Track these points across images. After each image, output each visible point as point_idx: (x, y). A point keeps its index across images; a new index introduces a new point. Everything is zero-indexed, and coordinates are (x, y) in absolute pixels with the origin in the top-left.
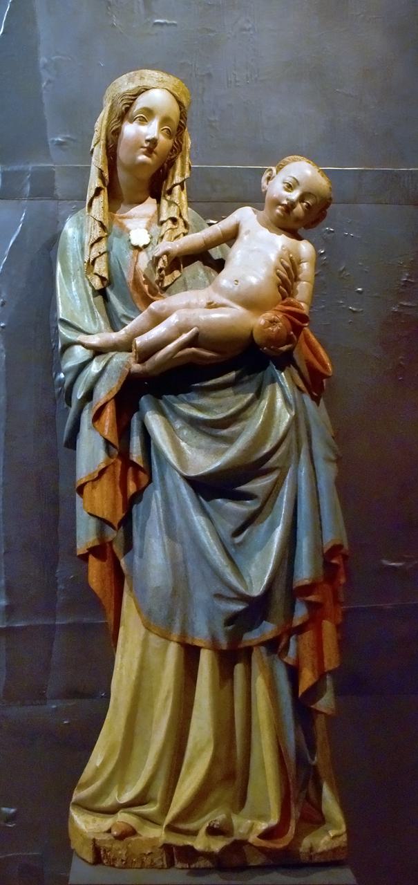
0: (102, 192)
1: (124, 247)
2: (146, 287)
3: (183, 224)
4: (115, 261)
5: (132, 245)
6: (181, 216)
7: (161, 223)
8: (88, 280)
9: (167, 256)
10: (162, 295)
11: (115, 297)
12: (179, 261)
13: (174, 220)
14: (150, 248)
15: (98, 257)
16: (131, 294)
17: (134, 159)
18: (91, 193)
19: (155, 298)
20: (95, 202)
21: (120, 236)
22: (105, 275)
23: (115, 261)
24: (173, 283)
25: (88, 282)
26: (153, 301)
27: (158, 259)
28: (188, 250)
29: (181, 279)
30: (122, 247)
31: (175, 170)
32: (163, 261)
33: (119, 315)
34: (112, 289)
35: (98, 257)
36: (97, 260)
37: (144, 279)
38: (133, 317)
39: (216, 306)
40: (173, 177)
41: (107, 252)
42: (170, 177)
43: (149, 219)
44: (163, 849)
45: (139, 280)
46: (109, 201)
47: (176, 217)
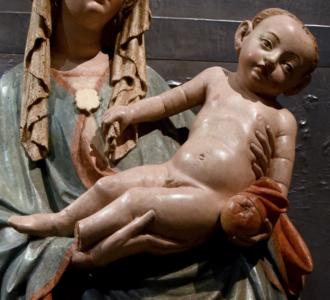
0: (44, 44)
1: (69, 110)
3: (140, 85)
4: (57, 128)
5: (78, 109)
6: (137, 75)
7: (113, 84)
8: (25, 149)
9: (120, 123)
10: (112, 169)
11: (55, 169)
13: (129, 81)
14: (99, 112)
15: (36, 122)
16: (75, 168)
17: (83, 6)
18: (30, 45)
19: (103, 173)
20: (35, 55)
21: (63, 97)
22: (45, 143)
23: (57, 128)
24: (125, 156)
25: (24, 152)
26: (101, 176)
27: (106, 127)
28: (145, 117)
29: (136, 151)
31: (131, 20)
33: (60, 192)
34: (52, 160)
35: (36, 122)
36: (36, 125)
37: (91, 150)
38: (76, 194)
39: (177, 185)
40: (129, 28)
41: (49, 116)
42: (126, 29)
43: (98, 78)
44: (52, 162)
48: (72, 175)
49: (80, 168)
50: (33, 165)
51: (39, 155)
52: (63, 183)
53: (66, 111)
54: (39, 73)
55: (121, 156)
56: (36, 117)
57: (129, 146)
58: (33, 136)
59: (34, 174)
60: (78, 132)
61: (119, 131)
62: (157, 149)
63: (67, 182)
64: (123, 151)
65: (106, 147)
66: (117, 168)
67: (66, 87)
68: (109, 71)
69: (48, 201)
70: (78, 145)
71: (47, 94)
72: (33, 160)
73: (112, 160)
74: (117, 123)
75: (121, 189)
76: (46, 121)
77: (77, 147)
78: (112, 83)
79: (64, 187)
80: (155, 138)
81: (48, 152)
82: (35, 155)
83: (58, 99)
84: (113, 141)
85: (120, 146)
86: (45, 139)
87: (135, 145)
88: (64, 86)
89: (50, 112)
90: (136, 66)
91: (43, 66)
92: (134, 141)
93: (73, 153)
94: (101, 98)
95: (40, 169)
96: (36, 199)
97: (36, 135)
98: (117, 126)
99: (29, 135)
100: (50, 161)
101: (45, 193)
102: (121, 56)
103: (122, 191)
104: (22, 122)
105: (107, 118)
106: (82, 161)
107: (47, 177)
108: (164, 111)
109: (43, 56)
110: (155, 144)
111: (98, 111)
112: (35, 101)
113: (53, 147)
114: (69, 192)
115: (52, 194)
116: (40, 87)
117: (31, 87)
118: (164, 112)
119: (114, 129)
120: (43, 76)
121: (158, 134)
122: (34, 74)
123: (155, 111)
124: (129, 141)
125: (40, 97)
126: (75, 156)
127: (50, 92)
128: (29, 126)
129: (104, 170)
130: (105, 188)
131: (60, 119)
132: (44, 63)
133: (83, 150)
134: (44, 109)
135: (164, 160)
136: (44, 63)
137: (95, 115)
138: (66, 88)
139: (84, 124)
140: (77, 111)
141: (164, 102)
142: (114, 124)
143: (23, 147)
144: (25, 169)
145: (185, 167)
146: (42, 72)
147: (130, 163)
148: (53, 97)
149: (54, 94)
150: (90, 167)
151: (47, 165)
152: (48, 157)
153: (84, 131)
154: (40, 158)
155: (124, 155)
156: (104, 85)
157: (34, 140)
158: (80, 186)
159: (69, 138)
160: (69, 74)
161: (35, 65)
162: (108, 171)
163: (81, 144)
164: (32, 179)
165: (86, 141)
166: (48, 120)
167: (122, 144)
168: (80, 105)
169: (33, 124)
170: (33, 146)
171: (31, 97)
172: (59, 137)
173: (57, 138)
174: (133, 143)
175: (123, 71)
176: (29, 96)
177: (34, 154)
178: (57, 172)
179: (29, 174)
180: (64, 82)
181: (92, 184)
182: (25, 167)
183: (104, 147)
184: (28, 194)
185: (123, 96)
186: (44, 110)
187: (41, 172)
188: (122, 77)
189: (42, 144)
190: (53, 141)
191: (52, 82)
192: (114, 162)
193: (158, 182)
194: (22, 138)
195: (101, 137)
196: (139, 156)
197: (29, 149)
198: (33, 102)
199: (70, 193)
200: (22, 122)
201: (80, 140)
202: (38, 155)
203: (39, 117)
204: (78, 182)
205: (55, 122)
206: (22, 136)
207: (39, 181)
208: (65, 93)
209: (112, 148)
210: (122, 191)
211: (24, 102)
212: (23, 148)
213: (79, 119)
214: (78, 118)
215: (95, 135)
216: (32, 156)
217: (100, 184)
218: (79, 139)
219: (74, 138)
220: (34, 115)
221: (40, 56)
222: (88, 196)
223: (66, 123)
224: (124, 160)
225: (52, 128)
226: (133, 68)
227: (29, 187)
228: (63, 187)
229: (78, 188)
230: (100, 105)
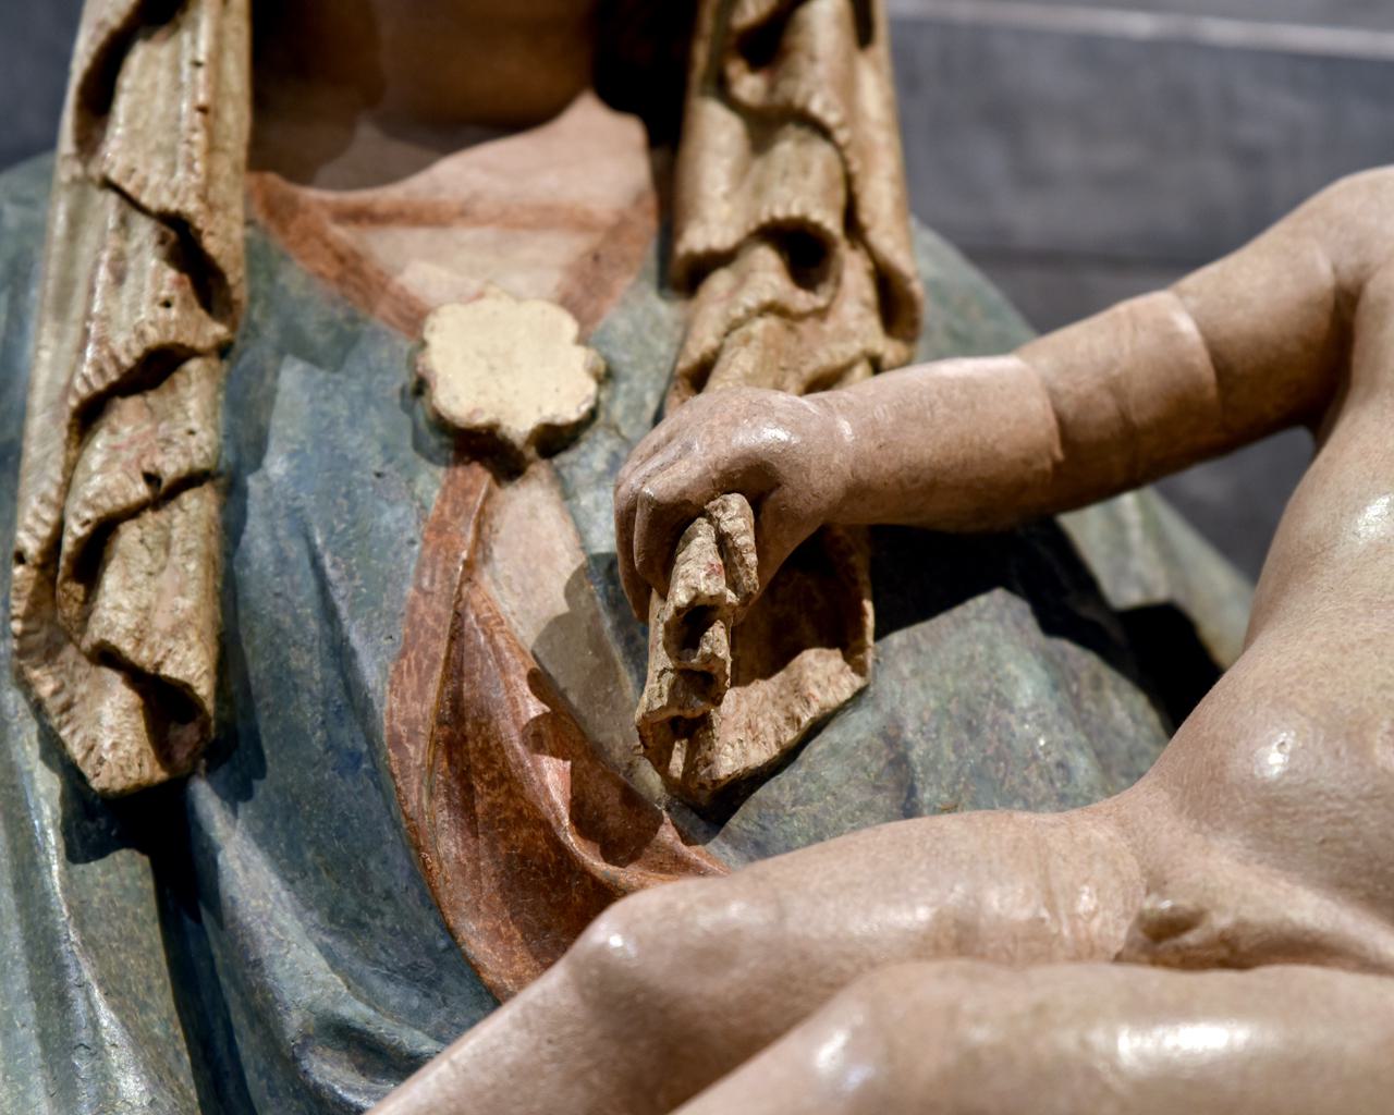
1: (372, 437)
2: (552, 777)
3: (869, 293)
4: (282, 560)
5: (442, 425)
6: (853, 225)
7: (686, 277)
8: (38, 707)
9: (757, 503)
10: (692, 853)
11: (258, 859)
12: (869, 562)
13: (804, 251)
14: (593, 455)
15: (133, 512)
16: (414, 843)
19: (626, 875)
20: (144, 67)
21: (337, 350)
22: (190, 665)
23: (282, 560)
24: (789, 756)
25: (32, 729)
26: (604, 895)
27: (662, 527)
28: (927, 484)
29: (858, 728)
30: (353, 441)
32: (723, 542)
33: (294, 1023)
34: (237, 793)
35: (133, 512)
36: (129, 534)
37: (534, 708)
38: (412, 1039)
39: (1239, 952)
41: (226, 480)
43: (580, 244)
44: (241, 806)
45: (485, 719)
46: (262, 100)
47: (816, 216)
48: (388, 895)
49: (448, 845)
50: (99, 821)
51: (141, 751)
52: (315, 954)
53: (353, 443)
54: (165, 178)
55: (759, 756)
56: (135, 482)
57: (815, 691)
58: (105, 614)
59: (100, 892)
60: (438, 586)
61: (752, 558)
62: (1012, 719)
63: (343, 949)
64: (774, 720)
65: (652, 684)
66: (728, 849)
67: (357, 288)
68: (651, 202)
69: (193, 1092)
70: (438, 674)
71: (218, 330)
72: (96, 784)
73: (693, 786)
74: (736, 502)
75: (792, 978)
76: (203, 513)
77: (432, 692)
78: (677, 272)
79: (324, 985)
80: (992, 646)
81: (209, 732)
82: (114, 746)
83: (300, 366)
84: (709, 634)
85: (746, 683)
86: (193, 638)
87: (859, 682)
88: (341, 280)
89: (238, 450)
90: (845, 162)
91: (194, 130)
92: (847, 659)
93: (402, 729)
94: (606, 358)
95: (146, 859)
96: (106, 1077)
97: (125, 603)
98: (740, 521)
99: (75, 608)
100: (224, 798)
101: (179, 1032)
102: (733, 105)
103: (798, 993)
104: (29, 521)
105: (662, 468)
106: (468, 789)
107: (198, 919)
108: (1059, 454)
109: (197, 64)
110: (992, 689)
111: (583, 447)
112: (131, 371)
113: (247, 690)
114: (359, 1023)
115: (231, 1042)
116: (171, 274)
117: (103, 274)
118: (1057, 465)
119: (713, 546)
120: (192, 196)
121: (1008, 622)
122: (129, 187)
123: (1002, 448)
124: (809, 656)
125: (171, 338)
126: (412, 749)
127: (242, 322)
128: (79, 541)
129: (633, 858)
130: (658, 970)
131: (307, 500)
132: (203, 110)
133: (472, 713)
134: (195, 425)
135: (1063, 798)
136: (203, 110)
137: (565, 472)
138: (357, 296)
139: (486, 530)
140: (433, 441)
141: (1053, 393)
142: (719, 514)
143: (27, 695)
144: (34, 856)
145: (1285, 816)
146: (190, 167)
147: (826, 811)
148: (256, 352)
149: (271, 331)
150: (525, 833)
151: (199, 828)
152: (208, 770)
153: (485, 577)
154: (150, 771)
155: (776, 751)
156: (623, 283)
157: (113, 639)
158: (449, 981)
159: (369, 624)
160: (380, 209)
161: (139, 124)
162: (660, 868)
163: (461, 673)
164: (81, 925)
165: (496, 648)
166: (223, 508)
167: (766, 675)
168: (456, 398)
169: (105, 531)
170: (101, 687)
171: (102, 342)
172: (295, 617)
173: (279, 630)
174: (842, 671)
175: (759, 191)
176: (86, 332)
177: (107, 743)
178: (275, 881)
179: (65, 890)
180: (341, 259)
181: (536, 958)
182: (32, 836)
183: (630, 691)
184: (43, 1037)
185: (767, 347)
186: (192, 433)
187: (149, 884)
188: (752, 227)
189: (169, 670)
190: (248, 651)
191: (257, 257)
192: (704, 798)
193: (1074, 930)
194: (25, 633)
195: (607, 623)
196: (882, 763)
197: (67, 707)
198: (113, 376)
199: (370, 1028)
200: (29, 521)
201: (452, 638)
202: (135, 750)
203: (151, 479)
204: (430, 950)
205: (268, 515)
206: (26, 618)
207: (139, 942)
208: (348, 327)
209: (701, 684)
210: (798, 1001)
211: (50, 383)
212: (23, 705)
213: (444, 500)
214: (437, 493)
215: (562, 607)
216: (93, 757)
217: (616, 941)
218: (444, 632)
219: (412, 624)
220: (118, 466)
221: (176, 69)
222: (524, 1034)
223: (353, 524)
224: (780, 788)
225: (246, 563)
226: (827, 168)
227: (54, 984)
228: (312, 982)
229: (427, 995)
230: (598, 402)
